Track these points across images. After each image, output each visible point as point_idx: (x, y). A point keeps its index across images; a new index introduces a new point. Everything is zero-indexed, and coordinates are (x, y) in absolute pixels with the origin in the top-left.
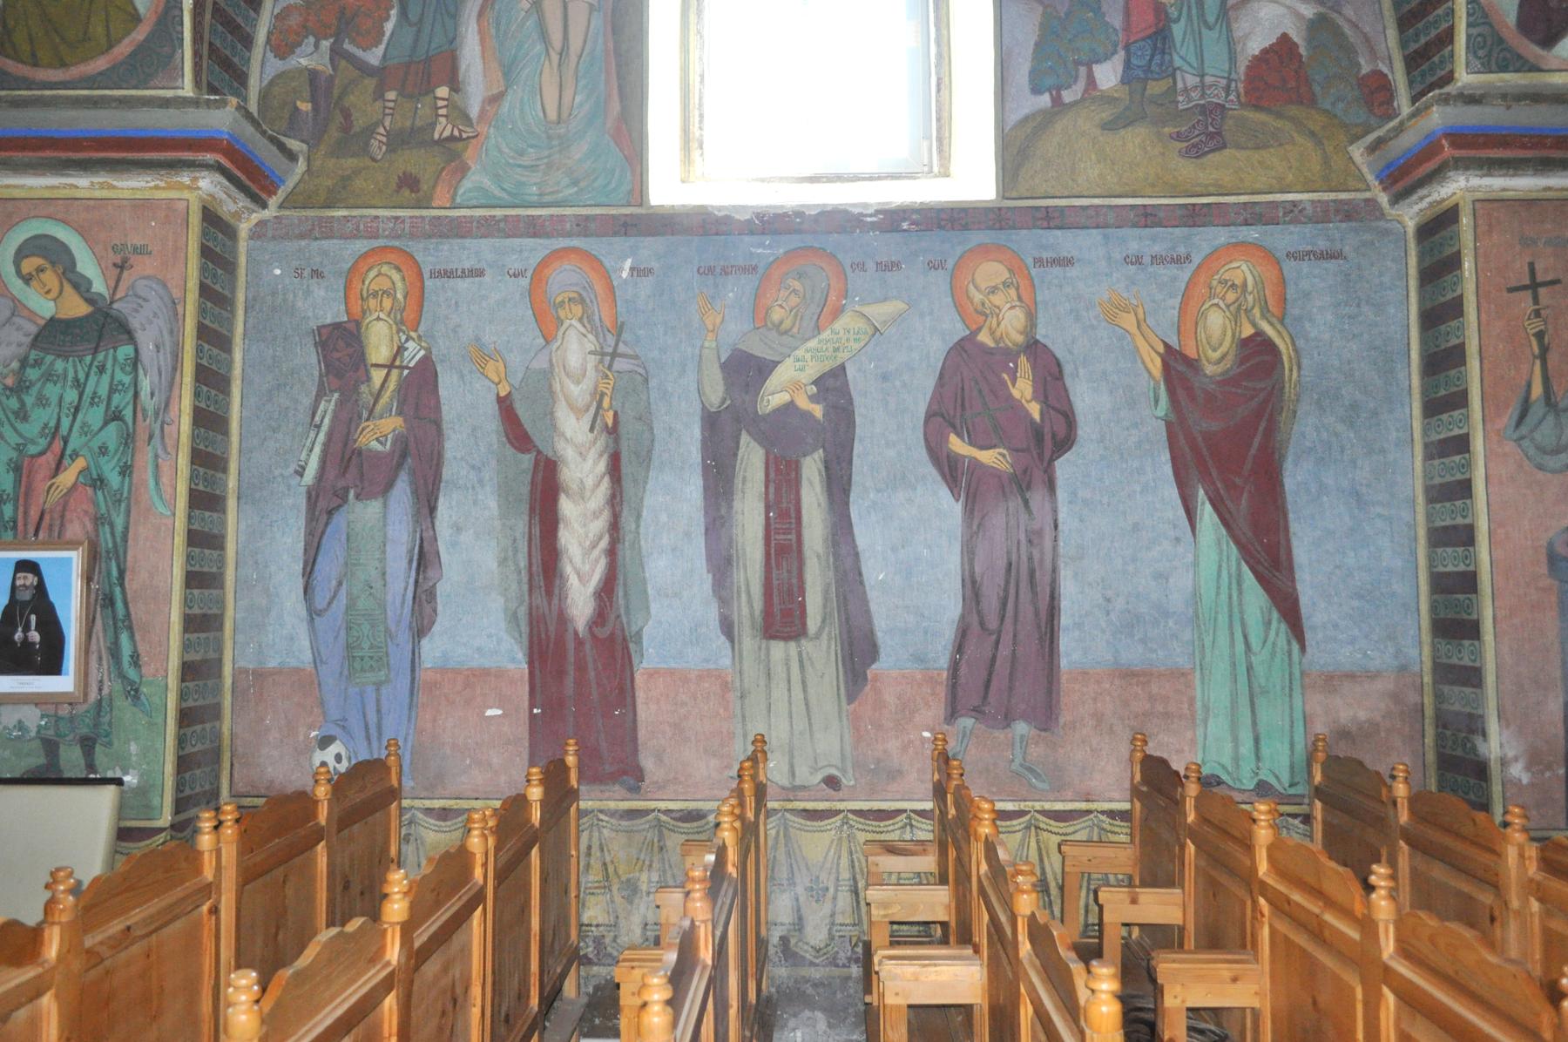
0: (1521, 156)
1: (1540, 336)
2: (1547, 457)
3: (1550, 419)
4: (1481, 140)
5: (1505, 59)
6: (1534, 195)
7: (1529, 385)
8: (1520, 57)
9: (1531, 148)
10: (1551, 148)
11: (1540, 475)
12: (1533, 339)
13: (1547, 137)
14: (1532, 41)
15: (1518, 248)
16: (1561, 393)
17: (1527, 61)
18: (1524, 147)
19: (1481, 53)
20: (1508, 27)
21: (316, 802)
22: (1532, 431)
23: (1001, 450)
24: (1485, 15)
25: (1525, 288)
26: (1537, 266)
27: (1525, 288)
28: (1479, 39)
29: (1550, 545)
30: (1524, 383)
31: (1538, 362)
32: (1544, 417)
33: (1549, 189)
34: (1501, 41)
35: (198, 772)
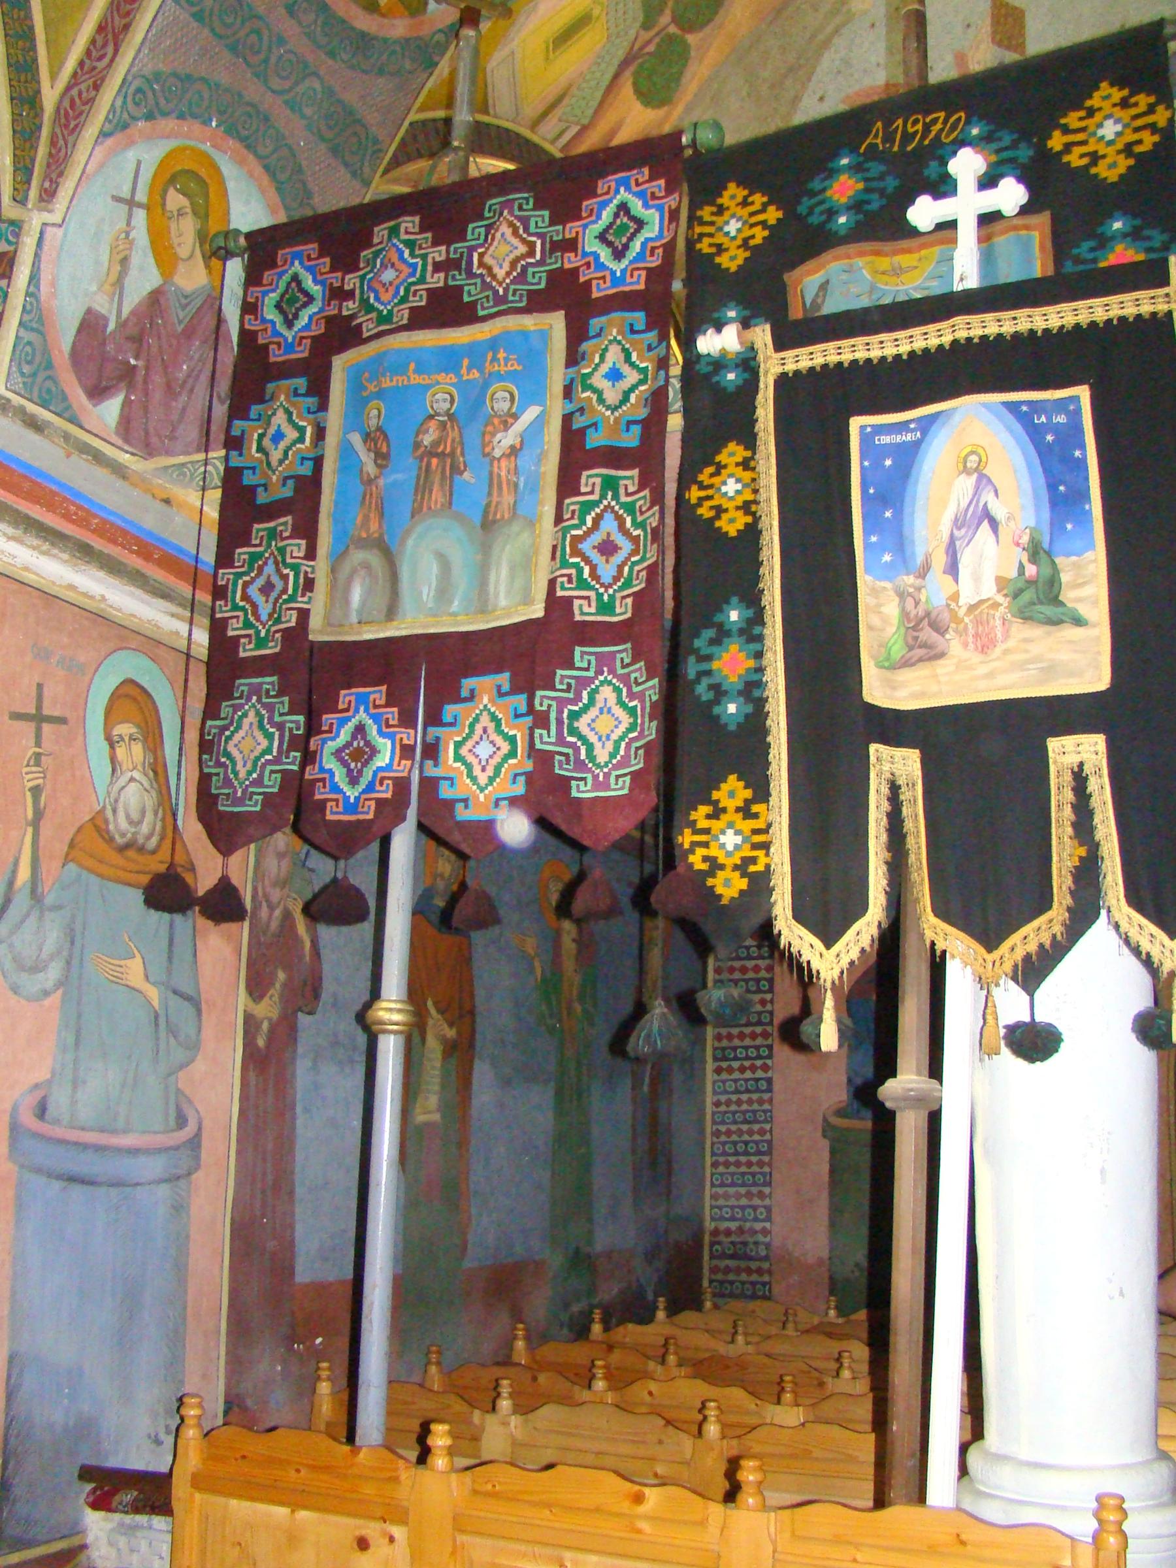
0: (59, 528)
1: (36, 791)
2: (24, 975)
3: (35, 914)
4: (27, 485)
5: (49, 391)
6: (54, 591)
7: (16, 864)
8: (65, 398)
9: (73, 522)
10: (94, 531)
11: (13, 999)
12: (28, 794)
13: (95, 516)
14: (80, 381)
15: (28, 659)
16: (50, 883)
17: (68, 408)
18: (67, 517)
19: (26, 369)
20: (61, 351)
21: (666, 1308)
22: (12, 933)
23: (471, 226)
24: (41, 320)
25: (39, 707)
26: (45, 690)
27: (39, 707)
28: (28, 349)
29: (15, 1109)
30: (11, 859)
31: (30, 830)
32: (28, 915)
33: (71, 587)
34: (50, 366)
35: (808, 1246)
